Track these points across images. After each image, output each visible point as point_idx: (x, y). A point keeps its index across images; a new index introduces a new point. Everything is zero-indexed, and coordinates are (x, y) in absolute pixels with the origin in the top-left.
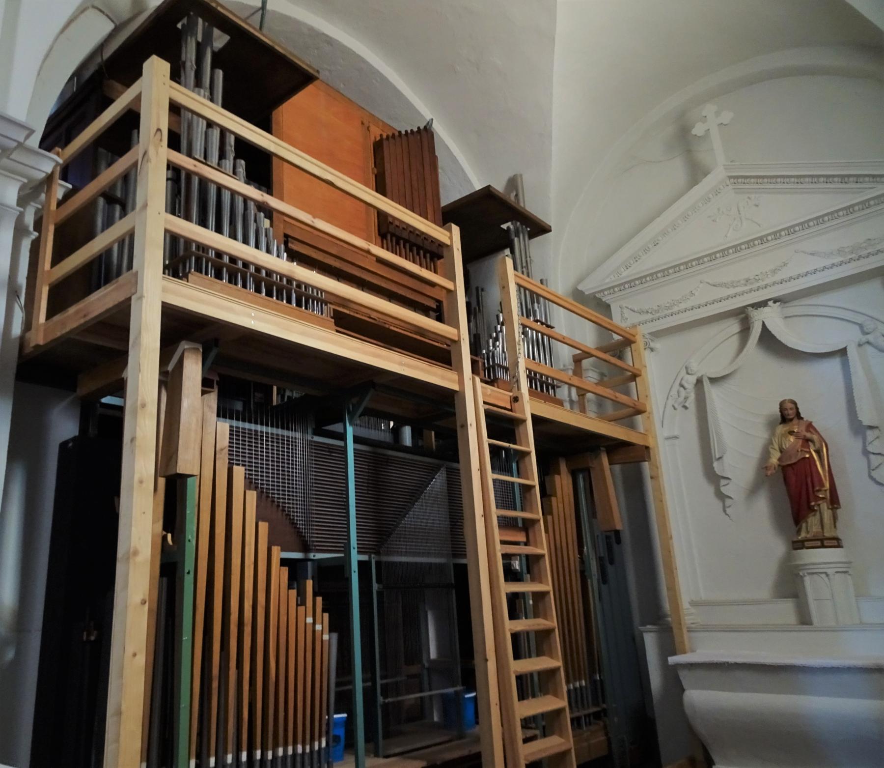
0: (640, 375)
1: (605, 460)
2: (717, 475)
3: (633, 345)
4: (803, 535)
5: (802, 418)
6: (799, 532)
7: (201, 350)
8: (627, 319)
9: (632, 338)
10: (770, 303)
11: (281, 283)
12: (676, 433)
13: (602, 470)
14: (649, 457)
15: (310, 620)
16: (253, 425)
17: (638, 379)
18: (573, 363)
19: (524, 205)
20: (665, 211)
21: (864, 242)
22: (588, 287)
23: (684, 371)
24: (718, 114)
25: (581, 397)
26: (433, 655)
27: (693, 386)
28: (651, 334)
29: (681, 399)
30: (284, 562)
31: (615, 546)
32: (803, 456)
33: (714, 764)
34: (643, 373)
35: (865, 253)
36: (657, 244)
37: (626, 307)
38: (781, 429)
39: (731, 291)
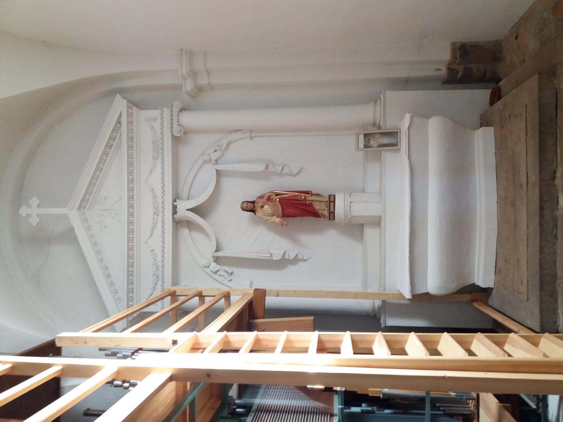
2: (281, 259)
4: (326, 213)
5: (254, 201)
6: (324, 216)
10: (175, 204)
21: (154, 145)
23: (206, 269)
24: (29, 206)
27: (218, 265)
29: (226, 274)
32: (278, 202)
35: (160, 146)
36: (107, 267)
38: (259, 213)
39: (159, 225)
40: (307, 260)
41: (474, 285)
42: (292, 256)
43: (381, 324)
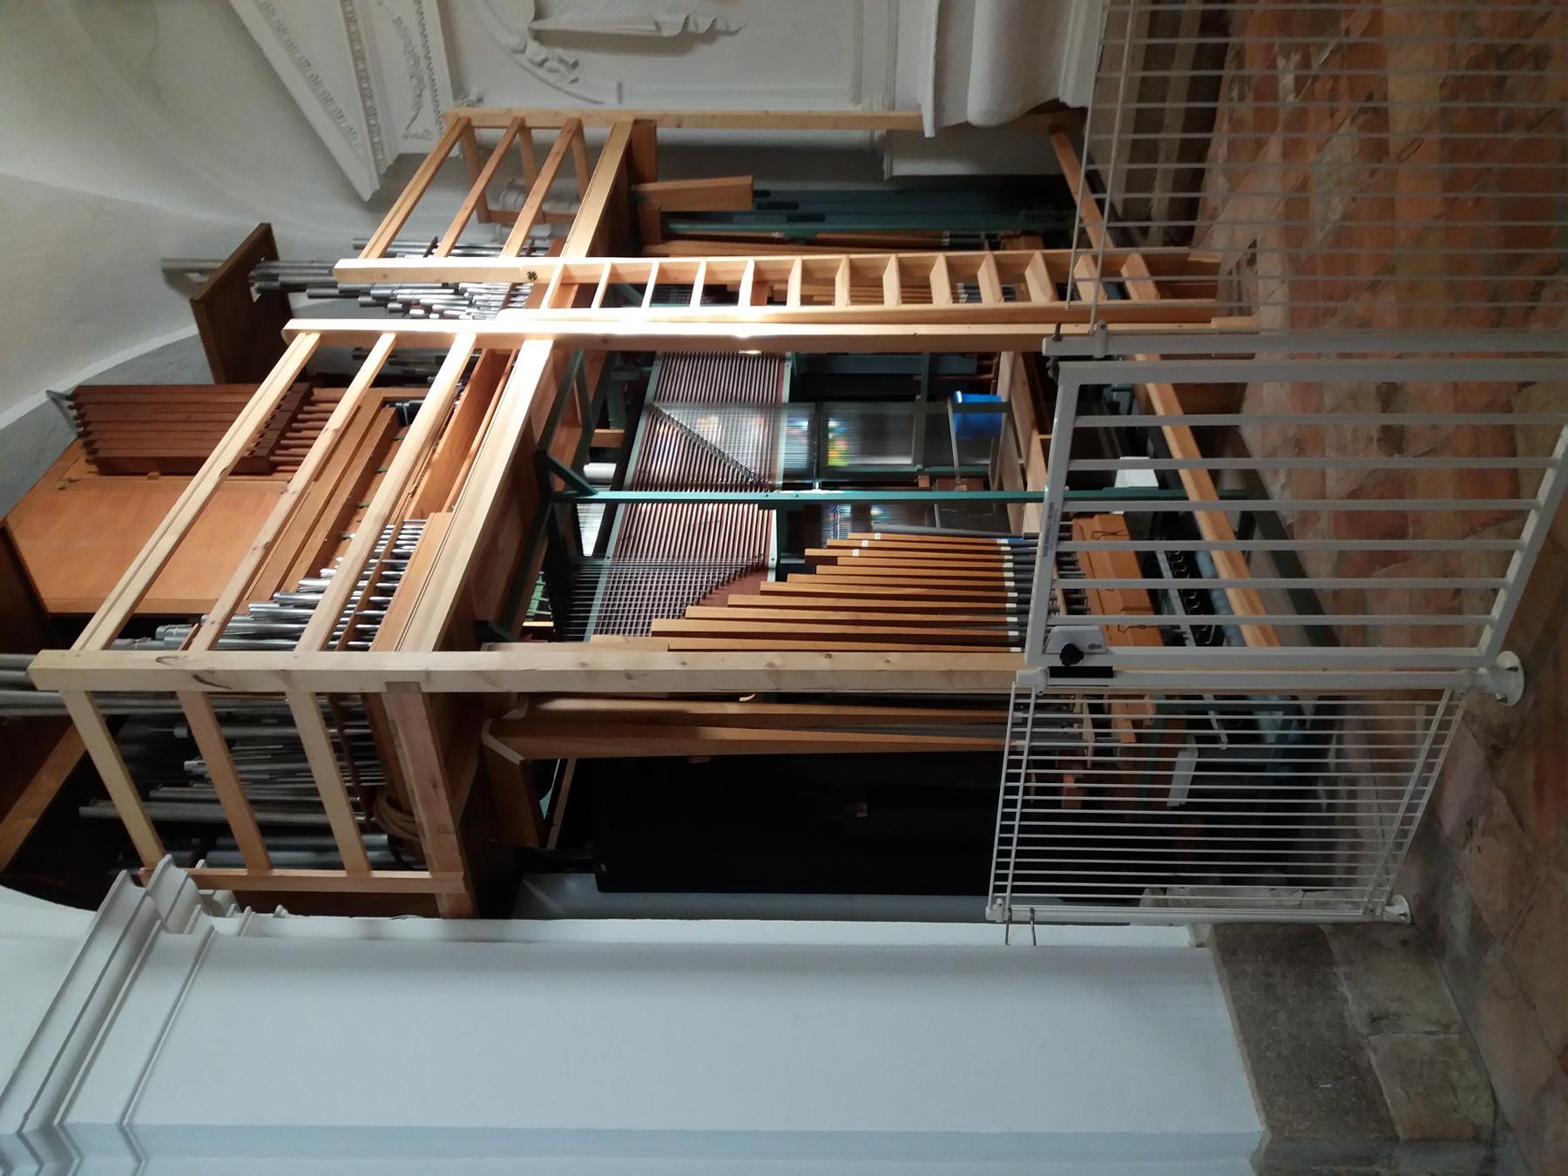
0: (523, 121)
1: (650, 187)
2: (680, 33)
3: (475, 123)
7: (491, 643)
8: (427, 130)
9: (462, 123)
11: (365, 589)
12: (614, 85)
13: (666, 192)
14: (651, 122)
15: (856, 553)
16: (588, 628)
17: (529, 123)
18: (492, 224)
19: (221, 261)
20: (252, 38)
22: (367, 185)
23: (518, 57)
25: (547, 218)
26: (907, 461)
27: (543, 47)
28: (455, 97)
29: (562, 68)
30: (781, 577)
31: (771, 199)
33: (1058, 99)
34: (520, 114)
37: (407, 128)
40: (737, 31)
41: (1056, 101)
42: (704, 26)
43: (883, 171)
